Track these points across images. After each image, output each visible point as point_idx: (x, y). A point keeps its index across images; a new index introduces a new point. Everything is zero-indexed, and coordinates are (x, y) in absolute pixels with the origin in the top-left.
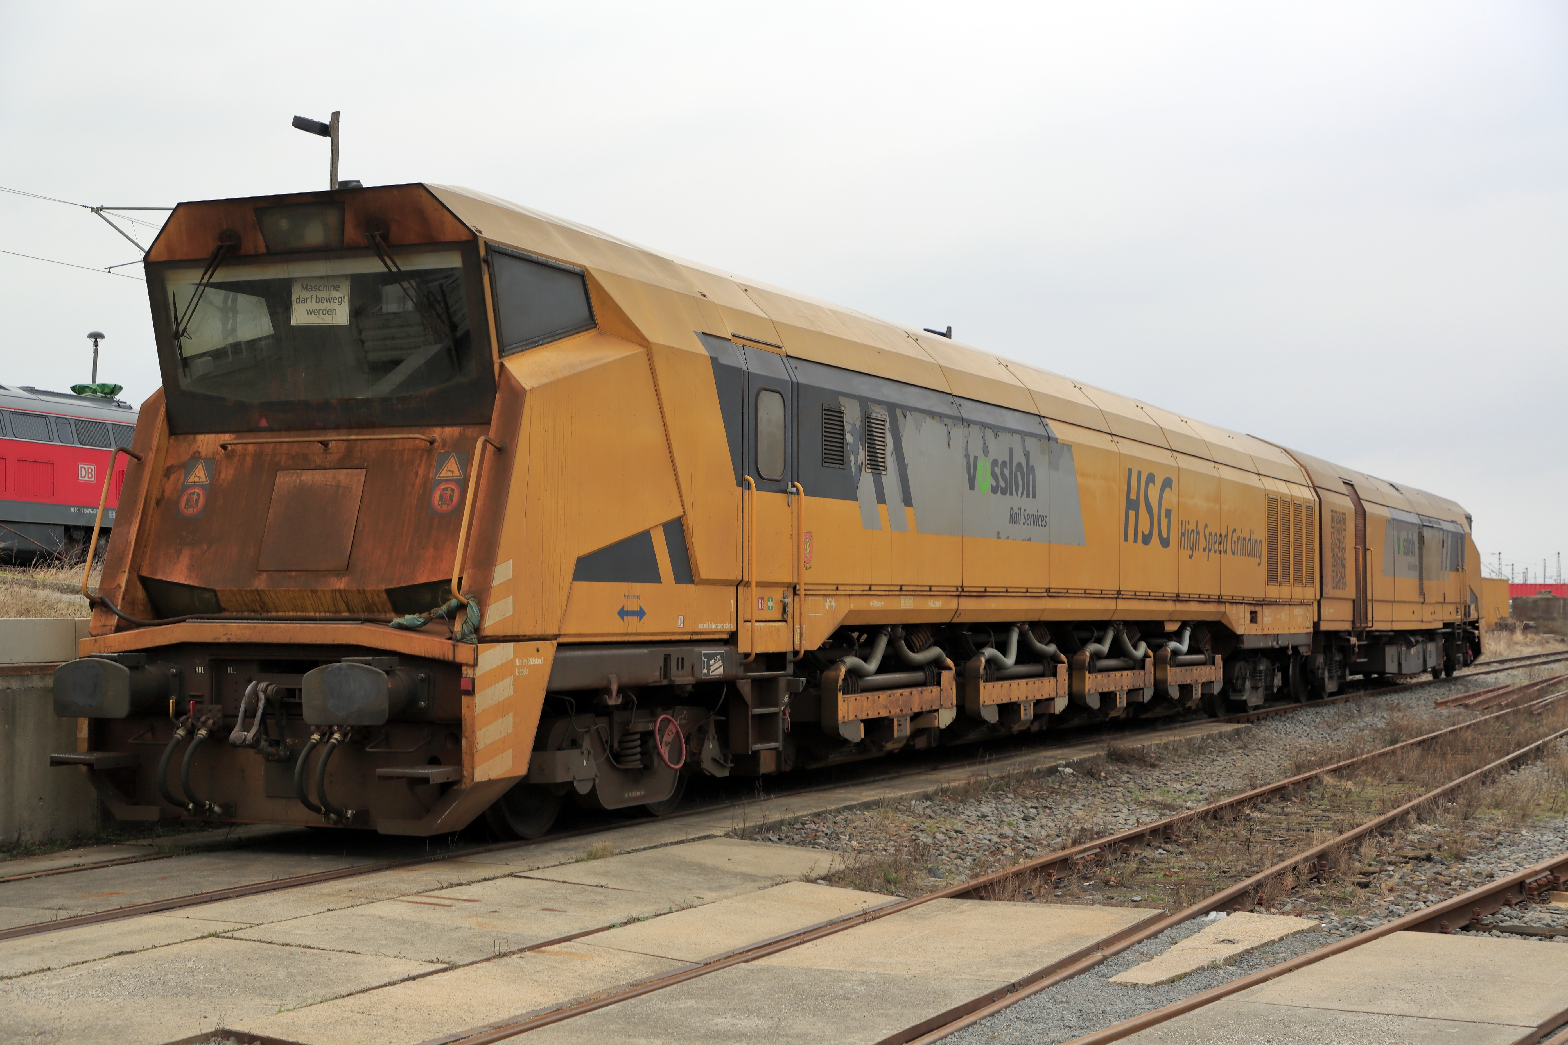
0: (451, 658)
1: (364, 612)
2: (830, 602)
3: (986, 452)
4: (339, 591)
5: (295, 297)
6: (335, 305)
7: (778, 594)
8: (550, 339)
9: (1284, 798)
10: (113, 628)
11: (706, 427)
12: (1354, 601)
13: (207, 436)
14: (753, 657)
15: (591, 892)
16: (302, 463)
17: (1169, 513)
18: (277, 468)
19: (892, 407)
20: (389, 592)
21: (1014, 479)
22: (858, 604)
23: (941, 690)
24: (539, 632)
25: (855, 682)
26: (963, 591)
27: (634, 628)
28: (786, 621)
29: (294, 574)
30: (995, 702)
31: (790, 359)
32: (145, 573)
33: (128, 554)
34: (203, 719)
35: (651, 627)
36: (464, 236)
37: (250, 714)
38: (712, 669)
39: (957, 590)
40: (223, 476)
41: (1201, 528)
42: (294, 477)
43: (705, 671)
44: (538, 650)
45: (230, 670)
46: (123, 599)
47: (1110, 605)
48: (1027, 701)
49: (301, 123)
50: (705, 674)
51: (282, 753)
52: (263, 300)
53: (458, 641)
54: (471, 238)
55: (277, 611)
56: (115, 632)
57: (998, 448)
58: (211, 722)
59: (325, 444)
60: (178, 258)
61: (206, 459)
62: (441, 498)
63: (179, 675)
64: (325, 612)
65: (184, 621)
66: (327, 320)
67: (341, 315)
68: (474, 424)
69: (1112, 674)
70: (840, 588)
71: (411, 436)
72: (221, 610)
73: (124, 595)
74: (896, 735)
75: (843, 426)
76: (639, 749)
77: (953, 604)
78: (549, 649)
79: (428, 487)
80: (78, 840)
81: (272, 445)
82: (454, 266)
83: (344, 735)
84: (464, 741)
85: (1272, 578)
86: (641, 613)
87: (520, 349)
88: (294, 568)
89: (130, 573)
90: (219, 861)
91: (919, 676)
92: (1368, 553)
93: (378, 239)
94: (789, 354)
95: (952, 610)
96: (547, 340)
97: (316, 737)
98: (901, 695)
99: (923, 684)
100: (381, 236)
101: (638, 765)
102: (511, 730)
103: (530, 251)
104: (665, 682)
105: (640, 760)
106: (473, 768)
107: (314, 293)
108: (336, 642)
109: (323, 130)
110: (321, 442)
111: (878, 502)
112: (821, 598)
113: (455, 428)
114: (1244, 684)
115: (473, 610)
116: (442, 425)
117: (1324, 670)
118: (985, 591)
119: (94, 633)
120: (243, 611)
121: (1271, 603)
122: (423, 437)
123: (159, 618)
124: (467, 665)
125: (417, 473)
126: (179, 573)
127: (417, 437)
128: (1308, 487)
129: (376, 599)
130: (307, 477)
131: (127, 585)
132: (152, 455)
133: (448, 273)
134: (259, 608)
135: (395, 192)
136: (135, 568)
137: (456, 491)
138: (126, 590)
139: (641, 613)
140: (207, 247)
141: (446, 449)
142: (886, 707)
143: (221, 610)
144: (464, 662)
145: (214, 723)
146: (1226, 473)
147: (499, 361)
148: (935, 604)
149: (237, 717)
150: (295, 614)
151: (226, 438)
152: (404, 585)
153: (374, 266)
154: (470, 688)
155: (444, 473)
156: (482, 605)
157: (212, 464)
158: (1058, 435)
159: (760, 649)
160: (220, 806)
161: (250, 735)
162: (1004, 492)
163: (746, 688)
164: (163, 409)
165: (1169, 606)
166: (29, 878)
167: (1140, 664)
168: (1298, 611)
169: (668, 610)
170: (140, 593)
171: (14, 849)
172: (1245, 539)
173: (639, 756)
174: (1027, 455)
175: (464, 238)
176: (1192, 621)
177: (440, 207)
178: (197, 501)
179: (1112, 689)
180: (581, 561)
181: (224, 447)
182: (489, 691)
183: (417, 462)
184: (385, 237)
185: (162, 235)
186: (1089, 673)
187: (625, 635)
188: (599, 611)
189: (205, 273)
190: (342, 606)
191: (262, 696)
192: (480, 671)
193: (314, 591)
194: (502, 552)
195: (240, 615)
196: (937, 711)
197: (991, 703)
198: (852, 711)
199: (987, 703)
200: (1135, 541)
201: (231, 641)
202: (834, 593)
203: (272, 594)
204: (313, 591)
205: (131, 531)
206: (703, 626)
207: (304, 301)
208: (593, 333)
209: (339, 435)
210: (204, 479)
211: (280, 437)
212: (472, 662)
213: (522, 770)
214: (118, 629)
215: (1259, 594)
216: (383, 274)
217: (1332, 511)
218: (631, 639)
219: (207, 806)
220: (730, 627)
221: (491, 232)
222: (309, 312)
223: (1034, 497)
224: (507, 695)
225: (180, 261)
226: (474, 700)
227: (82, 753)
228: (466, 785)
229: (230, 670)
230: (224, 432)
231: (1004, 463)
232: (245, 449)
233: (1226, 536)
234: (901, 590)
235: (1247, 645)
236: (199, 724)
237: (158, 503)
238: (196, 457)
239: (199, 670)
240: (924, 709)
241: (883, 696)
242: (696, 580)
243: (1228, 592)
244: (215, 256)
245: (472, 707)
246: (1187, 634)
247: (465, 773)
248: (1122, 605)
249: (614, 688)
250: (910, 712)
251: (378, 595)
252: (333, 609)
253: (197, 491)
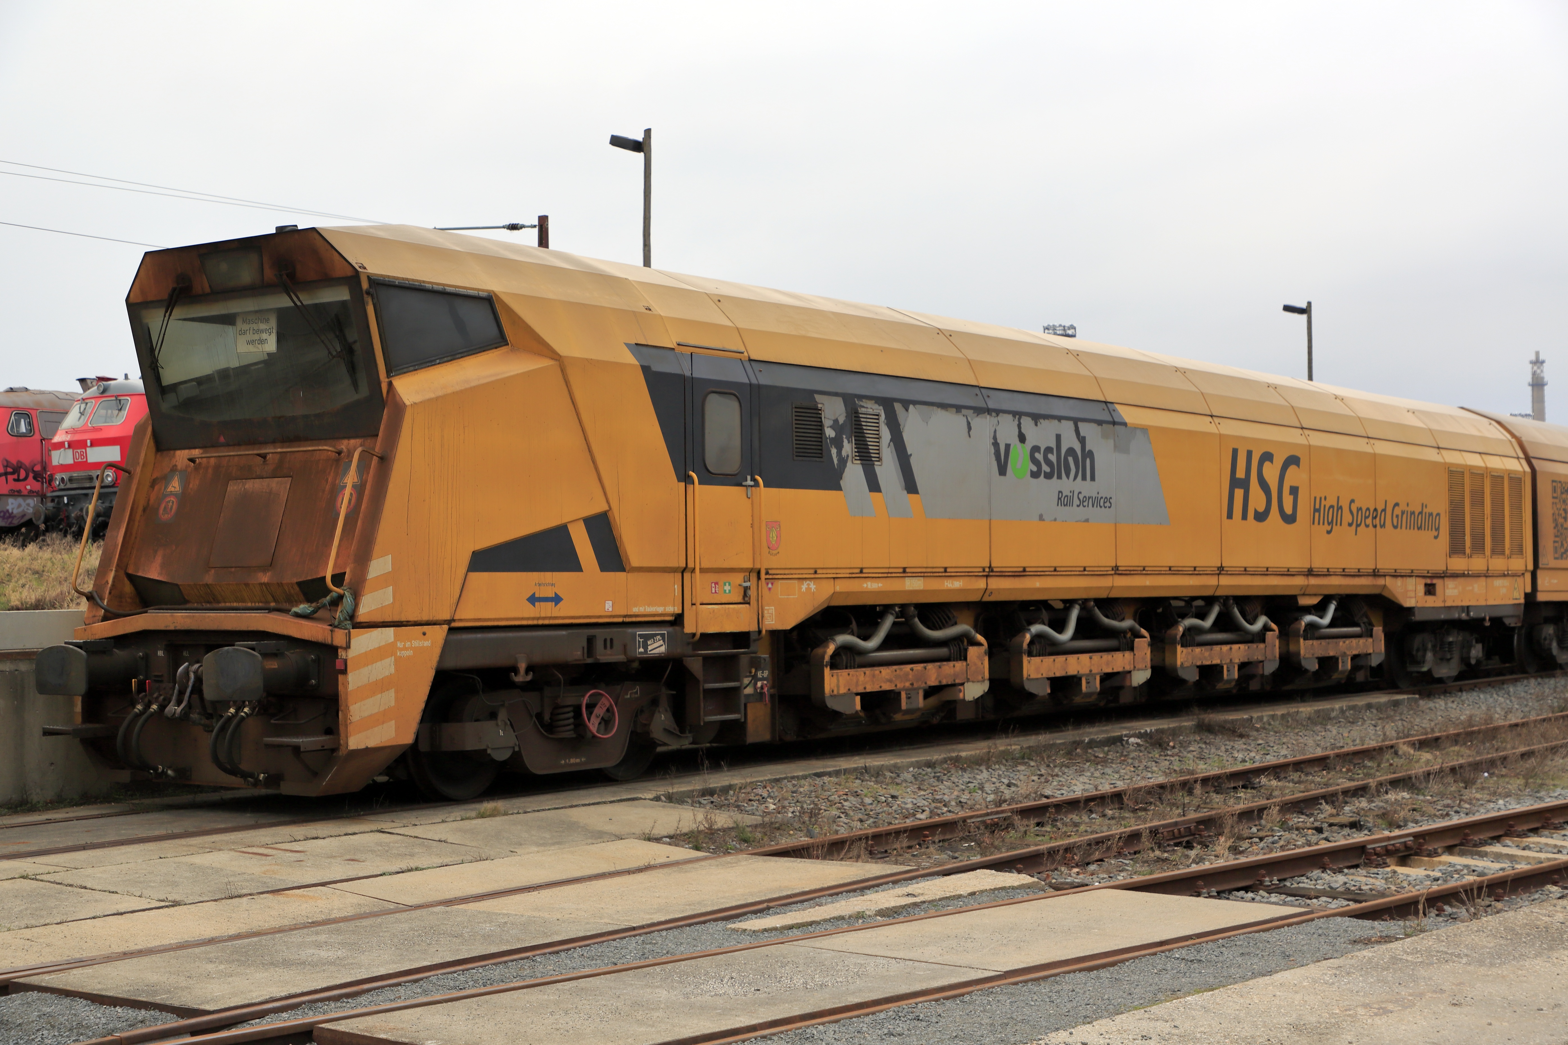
2: (808, 585)
3: (1022, 438)
4: (264, 584)
6: (264, 336)
7: (738, 579)
8: (449, 358)
9: (1326, 768)
11: (642, 429)
14: (698, 636)
16: (247, 474)
17: (1294, 491)
19: (887, 403)
20: (299, 584)
21: (1063, 463)
22: (841, 587)
23: (967, 665)
24: (425, 618)
25: (847, 658)
26: (992, 571)
27: (546, 612)
28: (749, 603)
29: (233, 569)
30: (1044, 676)
31: (753, 364)
32: (130, 571)
35: (566, 612)
36: (349, 273)
38: (650, 648)
39: (984, 571)
40: (191, 486)
41: (1345, 504)
43: (641, 650)
44: (424, 634)
46: (110, 593)
47: (1212, 581)
48: (1091, 674)
49: (618, 141)
50: (641, 653)
53: (336, 627)
55: (225, 602)
56: (102, 621)
57: (1041, 435)
59: (264, 456)
60: (150, 299)
63: (146, 658)
67: (271, 345)
69: (1217, 648)
70: (819, 571)
71: (320, 448)
72: (186, 602)
74: (904, 706)
75: (821, 422)
76: (572, 721)
77: (981, 584)
78: (439, 634)
80: (85, 799)
81: (227, 458)
84: (340, 713)
85: (1456, 548)
86: (557, 599)
87: (412, 368)
89: (116, 571)
90: (165, 816)
91: (943, 651)
93: (285, 277)
94: (752, 358)
95: (978, 589)
96: (446, 359)
97: (232, 710)
98: (912, 670)
99: (948, 659)
101: (571, 735)
102: (393, 704)
103: (424, 282)
104: (589, 661)
106: (347, 737)
107: (251, 326)
109: (637, 146)
110: (259, 455)
111: (871, 490)
112: (796, 581)
114: (1424, 656)
115: (348, 600)
118: (1024, 571)
121: (1455, 576)
122: (330, 449)
124: (341, 647)
127: (326, 448)
128: (1518, 458)
129: (292, 591)
131: (114, 581)
132: (139, 470)
133: (344, 303)
139: (557, 599)
142: (890, 681)
146: (1382, 448)
147: (387, 380)
148: (956, 584)
151: (196, 453)
156: (356, 596)
158: (1127, 420)
159: (701, 630)
160: (174, 770)
162: (1048, 476)
163: (695, 666)
164: (150, 429)
165: (1300, 581)
167: (1260, 637)
168: (1498, 582)
169: (586, 595)
170: (128, 588)
171: (21, 804)
172: (1413, 513)
174: (1082, 440)
176: (1339, 595)
177: (330, 247)
179: (1216, 661)
180: (475, 554)
181: (192, 460)
182: (365, 671)
186: (1182, 646)
187: (538, 619)
188: (506, 599)
189: (166, 312)
190: (270, 598)
191: (192, 676)
192: (352, 654)
194: (377, 549)
196: (963, 684)
197: (1040, 676)
198: (841, 686)
199: (1032, 676)
200: (1244, 517)
202: (812, 576)
206: (635, 610)
208: (504, 349)
210: (178, 489)
212: (344, 645)
213: (408, 738)
214: (105, 619)
215: (1440, 567)
217: (1553, 481)
218: (546, 622)
219: (160, 770)
221: (377, 266)
222: (248, 343)
223: (1093, 478)
224: (387, 674)
225: (152, 302)
228: (342, 752)
230: (195, 448)
231: (1049, 450)
232: (208, 462)
233: (1384, 510)
234: (904, 572)
235: (1418, 617)
237: (144, 510)
238: (174, 469)
240: (944, 682)
241: (886, 672)
242: (627, 568)
243: (1384, 565)
244: (171, 296)
246: (1332, 608)
247: (342, 742)
248: (1225, 581)
250: (923, 685)
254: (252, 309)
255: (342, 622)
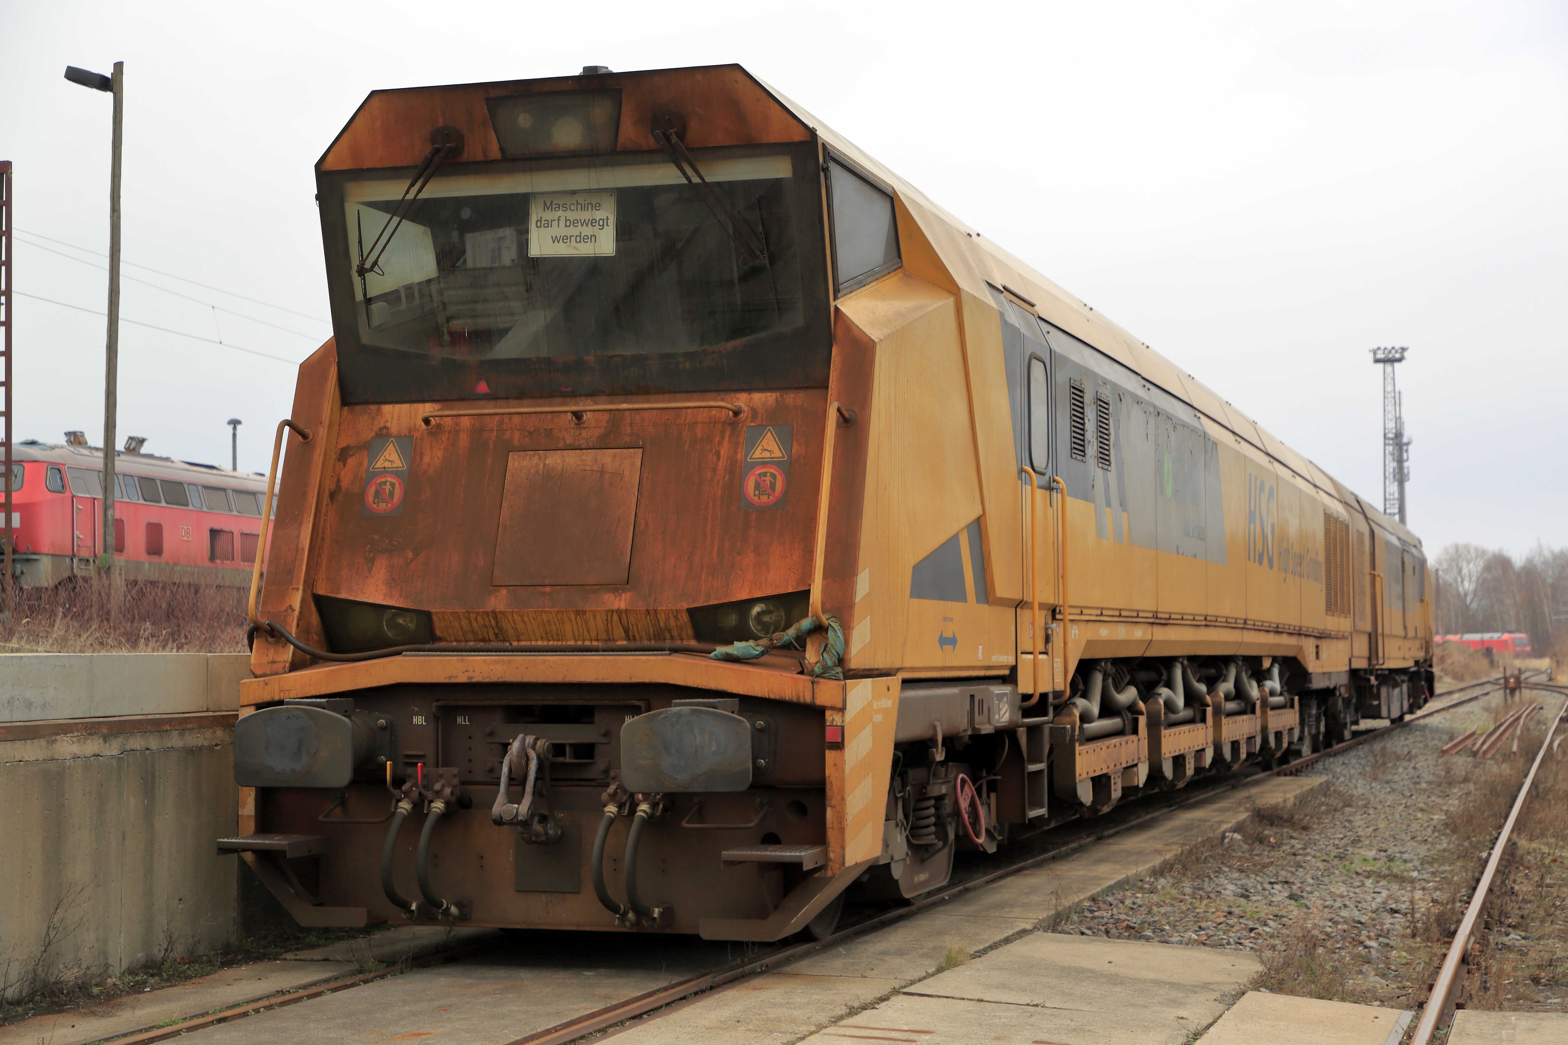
0: (808, 699)
1: (650, 640)
4: (619, 612)
5: (533, 218)
10: (288, 665)
12: (1370, 635)
13: (397, 406)
15: (1051, 1015)
16: (543, 441)
18: (507, 448)
20: (691, 612)
23: (1139, 740)
29: (548, 589)
32: (321, 591)
33: (301, 565)
34: (437, 786)
36: (798, 136)
37: (517, 781)
40: (426, 459)
42: (535, 460)
45: (460, 720)
46: (298, 625)
48: (1189, 753)
51: (551, 832)
52: (428, 230)
53: (817, 676)
54: (808, 139)
56: (291, 671)
58: (448, 791)
59: (578, 415)
61: (398, 437)
62: (757, 486)
63: (389, 728)
64: (591, 640)
65: (399, 653)
66: (586, 250)
67: (605, 244)
68: (796, 388)
72: (434, 638)
73: (298, 621)
79: (736, 472)
81: (497, 418)
82: (780, 176)
83: (654, 806)
84: (829, 812)
88: (547, 582)
89: (304, 590)
92: (1378, 580)
93: (674, 139)
97: (611, 809)
100: (676, 133)
105: (935, 833)
106: (843, 848)
107: (560, 213)
108: (634, 680)
113: (769, 394)
115: (835, 637)
116: (749, 390)
117: (1346, 714)
118: (1182, 619)
119: (258, 672)
120: (467, 641)
122: (729, 406)
123: (334, 651)
124: (833, 708)
125: (718, 454)
126: (373, 589)
127: (721, 404)
129: (672, 622)
130: (554, 459)
131: (301, 607)
132: (323, 432)
134: (492, 637)
135: (699, 76)
136: (309, 583)
137: (779, 477)
138: (301, 613)
140: (418, 149)
141: (759, 422)
143: (434, 638)
144: (828, 704)
145: (452, 793)
149: (498, 784)
150: (545, 643)
151: (427, 409)
152: (716, 602)
153: (664, 175)
154: (840, 741)
155: (758, 454)
156: (847, 628)
157: (408, 443)
161: (523, 808)
164: (333, 371)
166: (245, 1014)
170: (315, 619)
173: (933, 829)
175: (797, 138)
177: (765, 96)
178: (392, 493)
183: (717, 439)
184: (681, 136)
185: (345, 134)
189: (412, 185)
190: (619, 631)
191: (533, 755)
193: (579, 613)
195: (462, 645)
196: (1136, 765)
201: (474, 680)
203: (516, 617)
204: (577, 613)
205: (303, 534)
207: (548, 224)
209: (596, 403)
211: (509, 407)
214: (295, 666)
216: (679, 186)
220: (1010, 660)
222: (555, 240)
226: (843, 756)
227: (247, 836)
229: (460, 720)
232: (457, 424)
236: (429, 795)
237: (332, 496)
238: (383, 434)
239: (418, 720)
244: (428, 163)
245: (840, 767)
247: (832, 855)
249: (940, 739)
251: (676, 617)
252: (604, 636)
253: (389, 479)
254: (585, 186)
255: (830, 668)
